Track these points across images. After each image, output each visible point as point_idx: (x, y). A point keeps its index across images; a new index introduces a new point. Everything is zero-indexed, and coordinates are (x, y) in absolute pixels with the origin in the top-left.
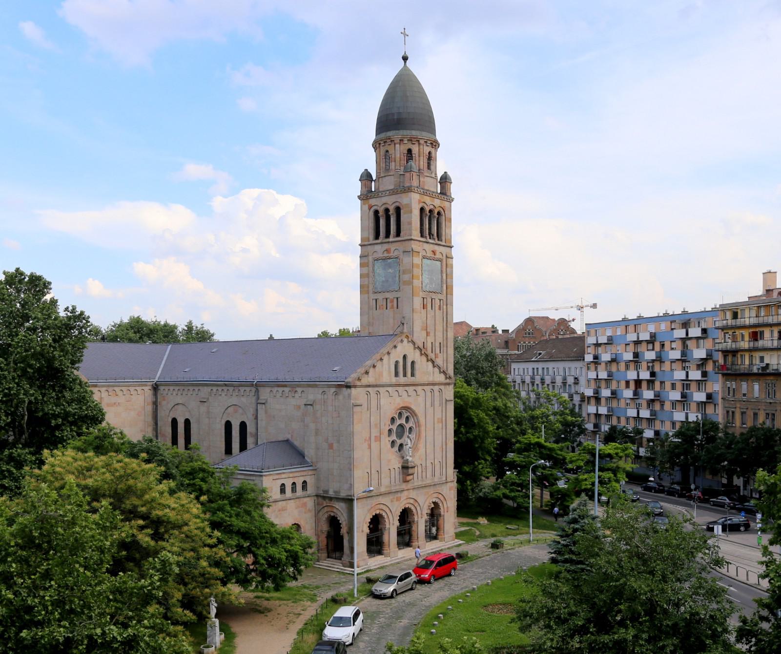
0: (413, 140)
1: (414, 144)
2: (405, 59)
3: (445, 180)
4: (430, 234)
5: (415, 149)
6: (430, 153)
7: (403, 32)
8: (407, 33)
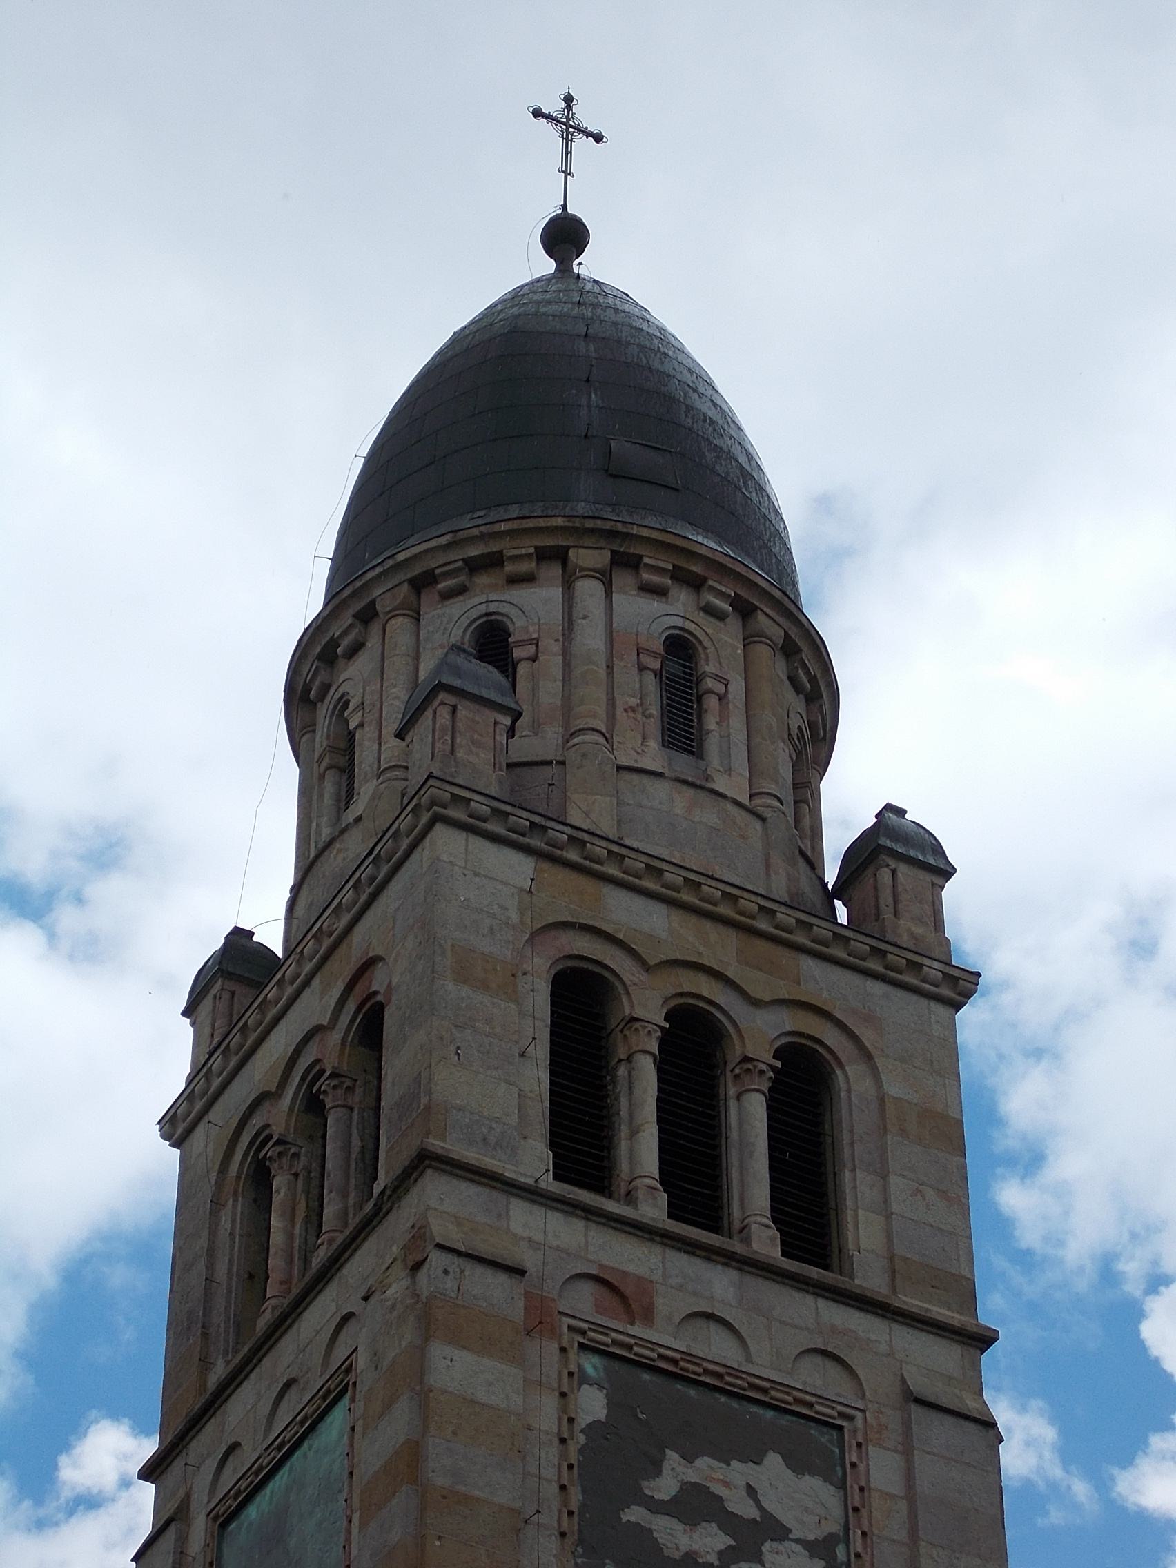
0: (507, 547)
1: (528, 579)
8: (583, 114)
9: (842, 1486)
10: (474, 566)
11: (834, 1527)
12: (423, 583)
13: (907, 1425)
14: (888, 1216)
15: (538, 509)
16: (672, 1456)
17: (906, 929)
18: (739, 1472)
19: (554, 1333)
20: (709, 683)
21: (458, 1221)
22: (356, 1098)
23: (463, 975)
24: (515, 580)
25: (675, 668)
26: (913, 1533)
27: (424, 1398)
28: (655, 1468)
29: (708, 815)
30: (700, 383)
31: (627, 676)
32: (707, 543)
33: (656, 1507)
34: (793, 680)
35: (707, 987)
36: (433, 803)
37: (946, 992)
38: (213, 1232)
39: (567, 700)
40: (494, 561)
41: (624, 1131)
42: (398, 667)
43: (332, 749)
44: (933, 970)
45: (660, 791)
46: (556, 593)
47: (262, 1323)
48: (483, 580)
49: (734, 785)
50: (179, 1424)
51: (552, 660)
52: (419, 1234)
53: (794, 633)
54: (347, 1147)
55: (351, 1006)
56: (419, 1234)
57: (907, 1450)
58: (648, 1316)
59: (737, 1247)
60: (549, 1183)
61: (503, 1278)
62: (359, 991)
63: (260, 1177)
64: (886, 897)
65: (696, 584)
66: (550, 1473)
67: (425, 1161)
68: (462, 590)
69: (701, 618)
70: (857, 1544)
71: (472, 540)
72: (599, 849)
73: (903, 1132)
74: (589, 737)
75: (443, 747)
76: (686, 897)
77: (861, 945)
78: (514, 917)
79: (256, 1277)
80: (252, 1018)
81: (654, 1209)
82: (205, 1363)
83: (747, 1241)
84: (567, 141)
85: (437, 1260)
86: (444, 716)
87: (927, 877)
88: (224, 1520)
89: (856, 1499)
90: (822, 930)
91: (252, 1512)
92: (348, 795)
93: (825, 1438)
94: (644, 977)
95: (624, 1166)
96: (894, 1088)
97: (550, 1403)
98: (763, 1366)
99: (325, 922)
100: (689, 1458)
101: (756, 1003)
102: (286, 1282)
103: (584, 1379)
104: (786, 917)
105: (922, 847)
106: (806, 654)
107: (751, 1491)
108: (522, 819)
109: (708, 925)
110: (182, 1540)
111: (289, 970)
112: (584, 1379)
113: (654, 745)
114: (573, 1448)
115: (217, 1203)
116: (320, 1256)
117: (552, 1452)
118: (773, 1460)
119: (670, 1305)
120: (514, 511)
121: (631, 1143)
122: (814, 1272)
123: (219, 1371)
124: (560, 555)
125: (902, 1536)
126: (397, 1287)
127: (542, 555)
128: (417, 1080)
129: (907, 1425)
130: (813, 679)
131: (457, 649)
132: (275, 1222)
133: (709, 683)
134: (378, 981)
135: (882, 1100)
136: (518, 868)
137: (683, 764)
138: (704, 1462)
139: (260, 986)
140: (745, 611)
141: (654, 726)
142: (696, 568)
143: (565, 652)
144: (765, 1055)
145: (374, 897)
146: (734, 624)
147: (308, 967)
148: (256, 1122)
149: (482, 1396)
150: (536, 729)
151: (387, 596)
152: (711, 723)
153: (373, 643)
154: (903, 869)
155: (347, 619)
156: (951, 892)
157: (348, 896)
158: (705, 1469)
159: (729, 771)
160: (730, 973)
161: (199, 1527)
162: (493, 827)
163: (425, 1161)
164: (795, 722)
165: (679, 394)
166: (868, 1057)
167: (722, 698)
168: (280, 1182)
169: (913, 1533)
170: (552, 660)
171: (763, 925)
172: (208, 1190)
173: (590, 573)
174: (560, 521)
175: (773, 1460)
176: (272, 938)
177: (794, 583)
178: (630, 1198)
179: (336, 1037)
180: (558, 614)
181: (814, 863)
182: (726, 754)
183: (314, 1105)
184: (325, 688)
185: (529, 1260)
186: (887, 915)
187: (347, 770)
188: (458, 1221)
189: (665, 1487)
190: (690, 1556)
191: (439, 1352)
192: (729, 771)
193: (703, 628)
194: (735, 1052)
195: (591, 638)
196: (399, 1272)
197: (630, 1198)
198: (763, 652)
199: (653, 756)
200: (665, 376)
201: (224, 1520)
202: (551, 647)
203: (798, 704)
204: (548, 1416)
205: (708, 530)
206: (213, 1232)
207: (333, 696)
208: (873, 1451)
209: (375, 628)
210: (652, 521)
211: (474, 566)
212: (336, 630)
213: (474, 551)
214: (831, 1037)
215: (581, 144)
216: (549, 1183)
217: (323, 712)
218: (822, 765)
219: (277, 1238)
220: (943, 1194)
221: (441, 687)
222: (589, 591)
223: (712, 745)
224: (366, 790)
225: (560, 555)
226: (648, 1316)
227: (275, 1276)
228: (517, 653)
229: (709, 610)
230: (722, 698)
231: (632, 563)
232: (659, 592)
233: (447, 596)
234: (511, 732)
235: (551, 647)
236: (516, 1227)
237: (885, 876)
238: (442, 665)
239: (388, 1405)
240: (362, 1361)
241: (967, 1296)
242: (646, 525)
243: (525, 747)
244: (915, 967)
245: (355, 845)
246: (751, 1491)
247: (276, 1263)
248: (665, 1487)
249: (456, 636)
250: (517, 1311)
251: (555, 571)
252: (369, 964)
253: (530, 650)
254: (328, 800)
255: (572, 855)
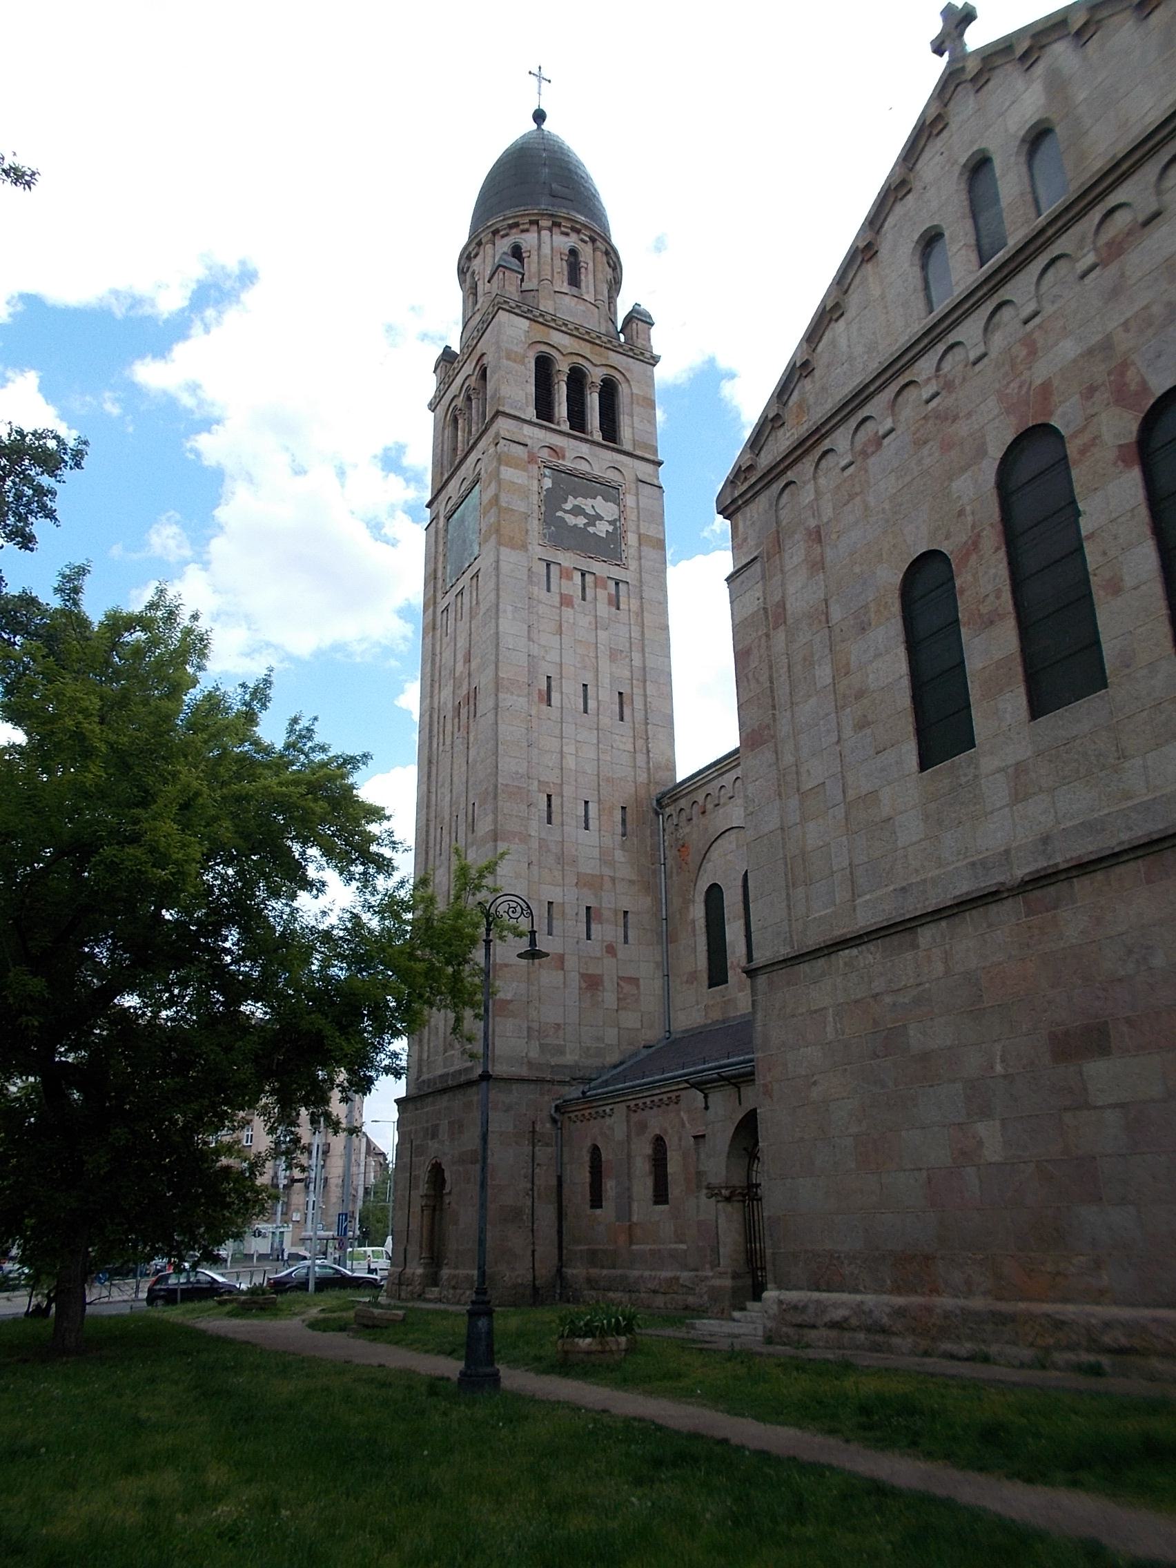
1: (527, 230)
2: (539, 116)
3: (639, 318)
4: (577, 419)
5: (528, 240)
6: (573, 252)
7: (536, 71)
8: (544, 74)
9: (619, 505)
10: (511, 227)
11: (617, 517)
12: (495, 233)
13: (637, 488)
14: (633, 428)
15: (530, 207)
16: (570, 497)
17: (640, 343)
18: (590, 501)
19: (536, 463)
20: (582, 264)
21: (508, 431)
22: (480, 396)
23: (508, 358)
24: (523, 231)
25: (572, 259)
26: (638, 518)
27: (499, 482)
28: (566, 501)
29: (582, 307)
30: (579, 165)
31: (557, 262)
32: (582, 218)
33: (566, 512)
34: (608, 263)
35: (581, 361)
36: (499, 303)
37: (651, 361)
38: (443, 436)
39: (539, 271)
40: (516, 225)
41: (557, 404)
42: (489, 260)
43: (471, 288)
44: (648, 355)
45: (567, 299)
46: (536, 235)
47: (456, 463)
48: (514, 231)
49: (589, 297)
50: (435, 493)
51: (534, 257)
52: (497, 435)
53: (609, 248)
54: (478, 411)
55: (478, 368)
56: (497, 435)
57: (637, 495)
58: (563, 458)
59: (589, 438)
60: (535, 420)
61: (521, 447)
62: (480, 363)
63: (455, 420)
64: (634, 333)
65: (578, 231)
66: (535, 502)
67: (498, 413)
68: (507, 235)
69: (580, 243)
70: (623, 521)
71: (509, 218)
72: (548, 317)
73: (638, 403)
74: (546, 282)
75: (501, 285)
76: (575, 333)
77: (627, 347)
78: (523, 339)
79: (455, 449)
80: (451, 373)
81: (565, 427)
82: (442, 474)
83: (592, 436)
84: (540, 82)
85: (502, 442)
86: (501, 274)
87: (647, 326)
88: (448, 518)
89: (622, 509)
90: (615, 343)
91: (455, 516)
92: (476, 302)
93: (614, 492)
94: (562, 357)
95: (557, 415)
96: (635, 391)
97: (536, 482)
98: (597, 472)
99: (469, 343)
100: (575, 498)
101: (596, 365)
102: (463, 450)
103: (545, 476)
104: (604, 339)
105: (645, 316)
106: (612, 255)
107: (593, 507)
108: (525, 308)
109: (581, 342)
110: (437, 523)
111: (460, 358)
112: (545, 476)
113: (565, 284)
114: (542, 495)
115: (444, 428)
116: (471, 442)
117: (536, 497)
118: (599, 498)
119: (570, 455)
120: (522, 208)
121: (749, 1177)
122: (611, 445)
123: (446, 476)
124: (536, 223)
125: (635, 519)
126: (492, 450)
127: (531, 222)
128: (496, 390)
129: (637, 488)
130: (614, 263)
131: (505, 253)
132: (459, 433)
133: (582, 264)
134: (485, 360)
135: (632, 394)
136: (524, 324)
137: (574, 290)
138: (579, 499)
139: (453, 363)
140: (593, 240)
141: (566, 278)
142: (578, 226)
143: (539, 255)
144: (598, 382)
145: (483, 334)
146: (590, 244)
147: (466, 357)
148: (453, 405)
149: (516, 481)
150: (530, 279)
151: (486, 237)
152: (583, 277)
153: (481, 253)
154: (640, 323)
155: (473, 245)
156: (653, 331)
157: (475, 333)
158: (580, 501)
159: (588, 293)
160: (588, 356)
161: (442, 520)
162: (516, 311)
163: (498, 413)
164: (609, 277)
165: (573, 168)
166: (628, 381)
167: (586, 269)
168: (460, 421)
169: (638, 518)
170: (534, 257)
171: (597, 341)
172: (441, 425)
173: (545, 229)
174: (536, 211)
175: (599, 498)
176: (456, 348)
177: (609, 231)
178: (558, 424)
179: (474, 378)
180: (536, 241)
181: (614, 323)
182: (587, 287)
183: (469, 399)
184: (468, 268)
185: (529, 442)
186: (635, 338)
187: (475, 294)
188: (508, 431)
189: (568, 506)
190: (575, 525)
191: (503, 468)
192: (588, 293)
193: (580, 246)
194: (590, 380)
195: (546, 250)
196: (492, 445)
197: (558, 424)
198: (599, 254)
199: (565, 288)
200: (569, 162)
201: (448, 518)
202: (534, 253)
203: (610, 271)
204: (535, 486)
205: (581, 214)
206: (443, 436)
207: (471, 270)
208: (627, 495)
209: (482, 247)
210: (564, 210)
211: (511, 227)
212: (470, 249)
213: (510, 222)
214: (618, 376)
215: (544, 83)
216: (535, 420)
217: (468, 274)
218: (618, 291)
219: (460, 438)
220: (649, 422)
221: (500, 266)
222: (545, 233)
223: (583, 285)
224: (480, 300)
225: (536, 223)
226: (563, 458)
227: (460, 449)
228: (524, 255)
229: (582, 240)
230: (586, 269)
231: (559, 225)
232: (567, 234)
233: (503, 237)
234: (522, 280)
235: (534, 253)
236: (525, 433)
237: (634, 325)
238: (501, 259)
239: (489, 485)
240: (483, 472)
241: (655, 450)
242: (562, 212)
243: (525, 286)
244: (642, 354)
245: (478, 317)
246: (593, 507)
247: (459, 445)
248: (568, 506)
249: (505, 249)
250: (525, 456)
251: (535, 228)
252: (483, 354)
253: (528, 254)
254: (470, 304)
255: (541, 320)
